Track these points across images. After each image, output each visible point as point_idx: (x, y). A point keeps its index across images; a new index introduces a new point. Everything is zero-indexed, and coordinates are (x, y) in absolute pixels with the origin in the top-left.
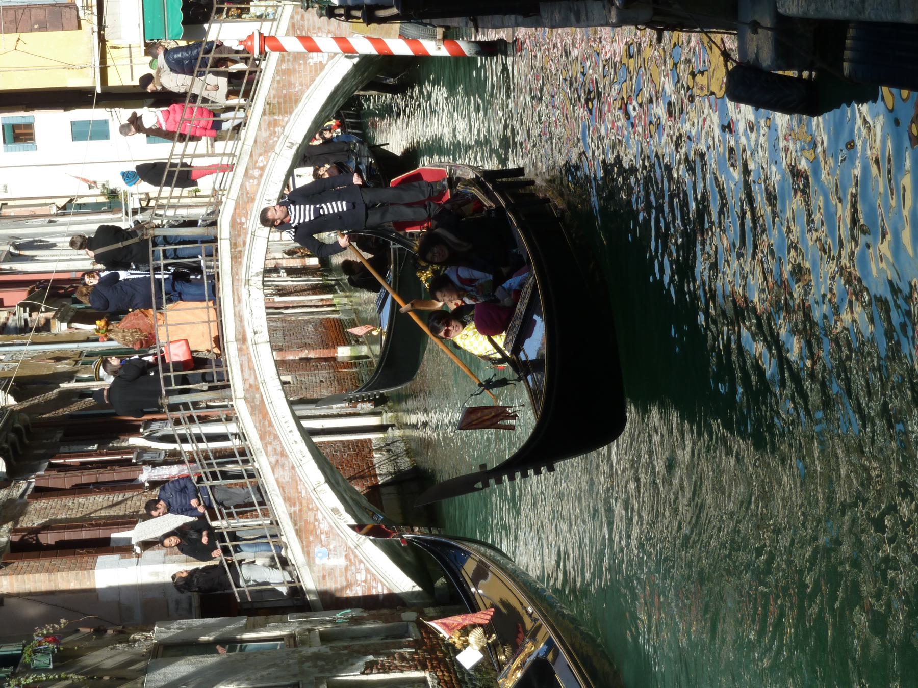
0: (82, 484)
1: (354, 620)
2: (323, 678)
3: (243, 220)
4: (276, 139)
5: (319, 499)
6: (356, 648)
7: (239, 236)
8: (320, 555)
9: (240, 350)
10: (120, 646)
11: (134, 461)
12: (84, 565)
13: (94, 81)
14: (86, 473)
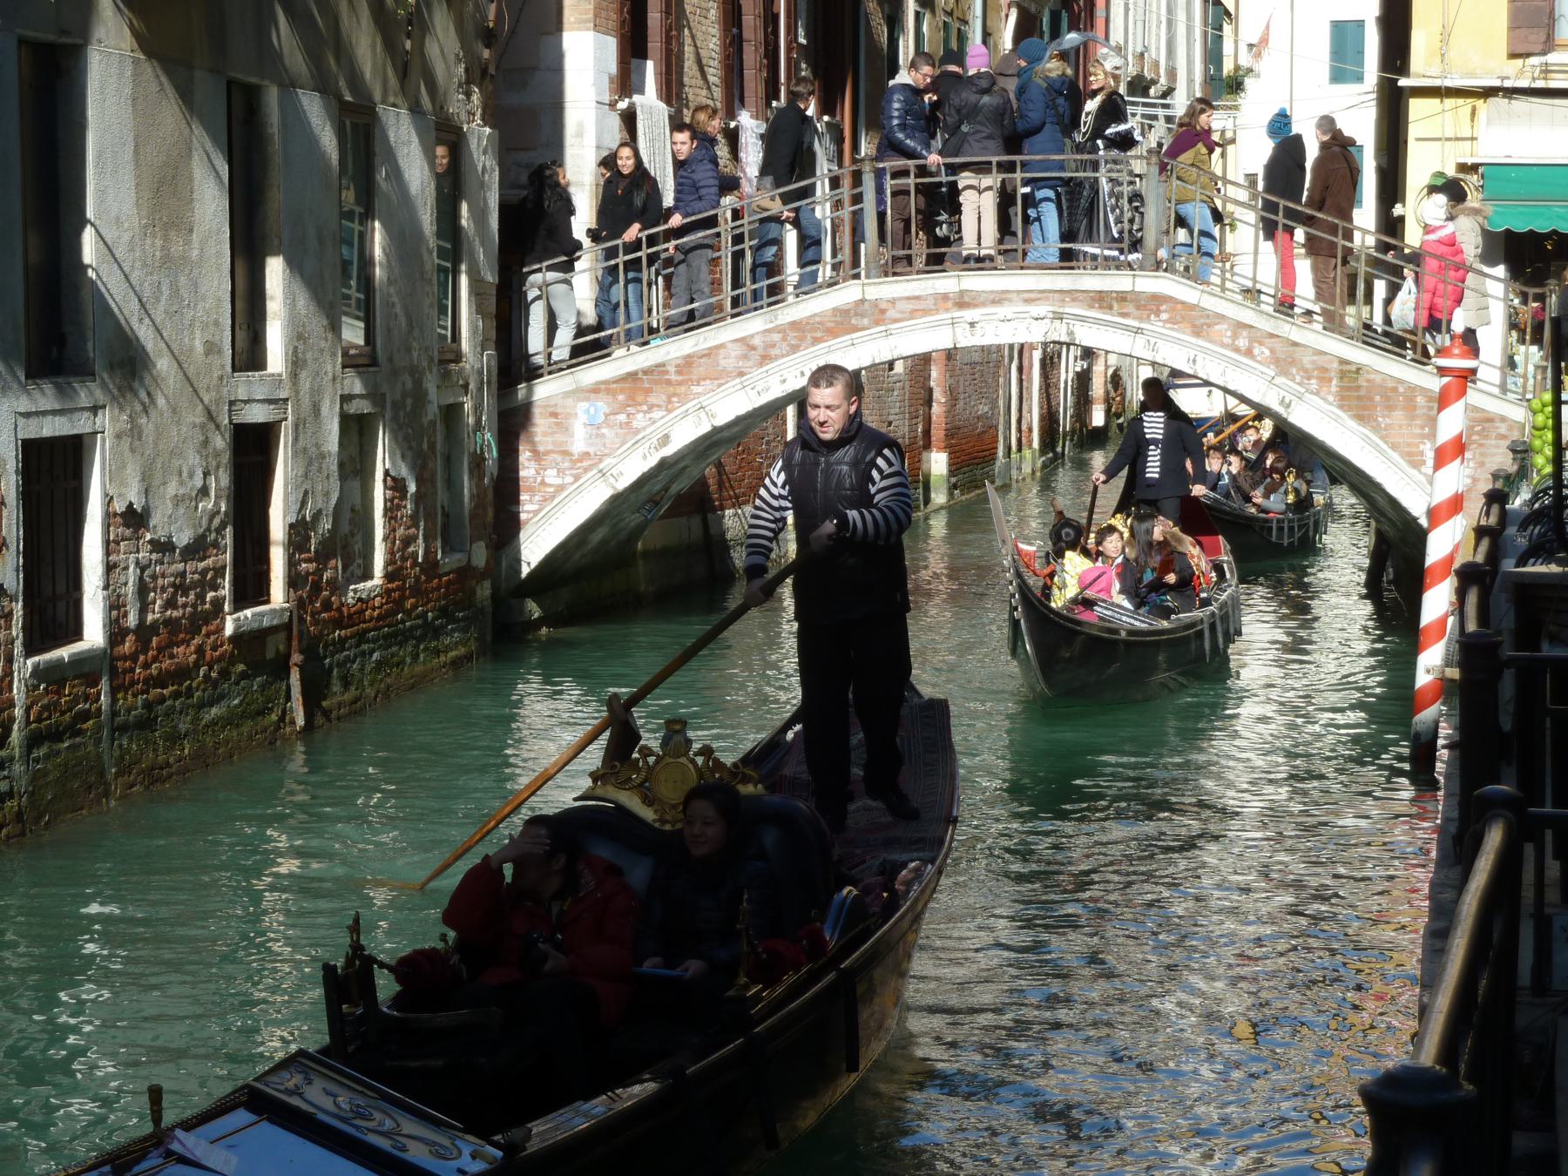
0: (740, 15)
1: (478, 462)
2: (383, 407)
3: (1164, 316)
4: (1298, 379)
5: (686, 414)
6: (431, 465)
7: (1138, 308)
8: (592, 410)
9: (945, 297)
10: (461, 69)
11: (774, 104)
12: (604, 14)
13: (1419, 76)
14: (760, 23)
